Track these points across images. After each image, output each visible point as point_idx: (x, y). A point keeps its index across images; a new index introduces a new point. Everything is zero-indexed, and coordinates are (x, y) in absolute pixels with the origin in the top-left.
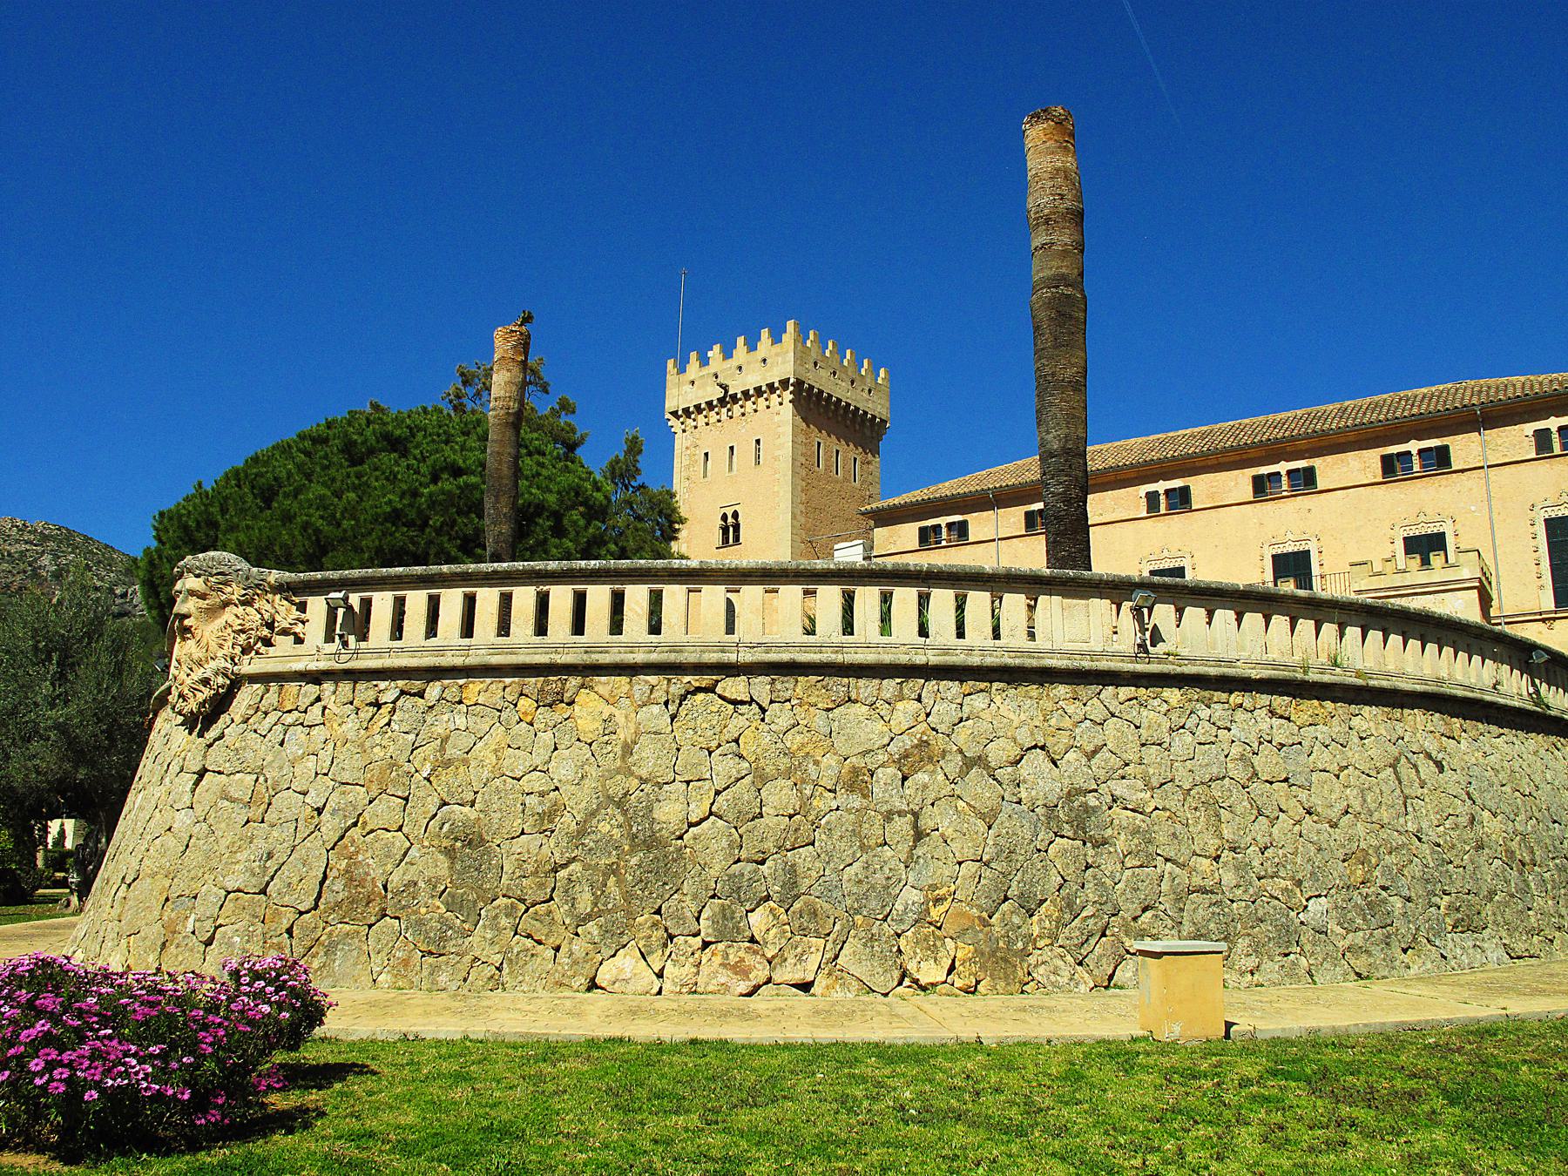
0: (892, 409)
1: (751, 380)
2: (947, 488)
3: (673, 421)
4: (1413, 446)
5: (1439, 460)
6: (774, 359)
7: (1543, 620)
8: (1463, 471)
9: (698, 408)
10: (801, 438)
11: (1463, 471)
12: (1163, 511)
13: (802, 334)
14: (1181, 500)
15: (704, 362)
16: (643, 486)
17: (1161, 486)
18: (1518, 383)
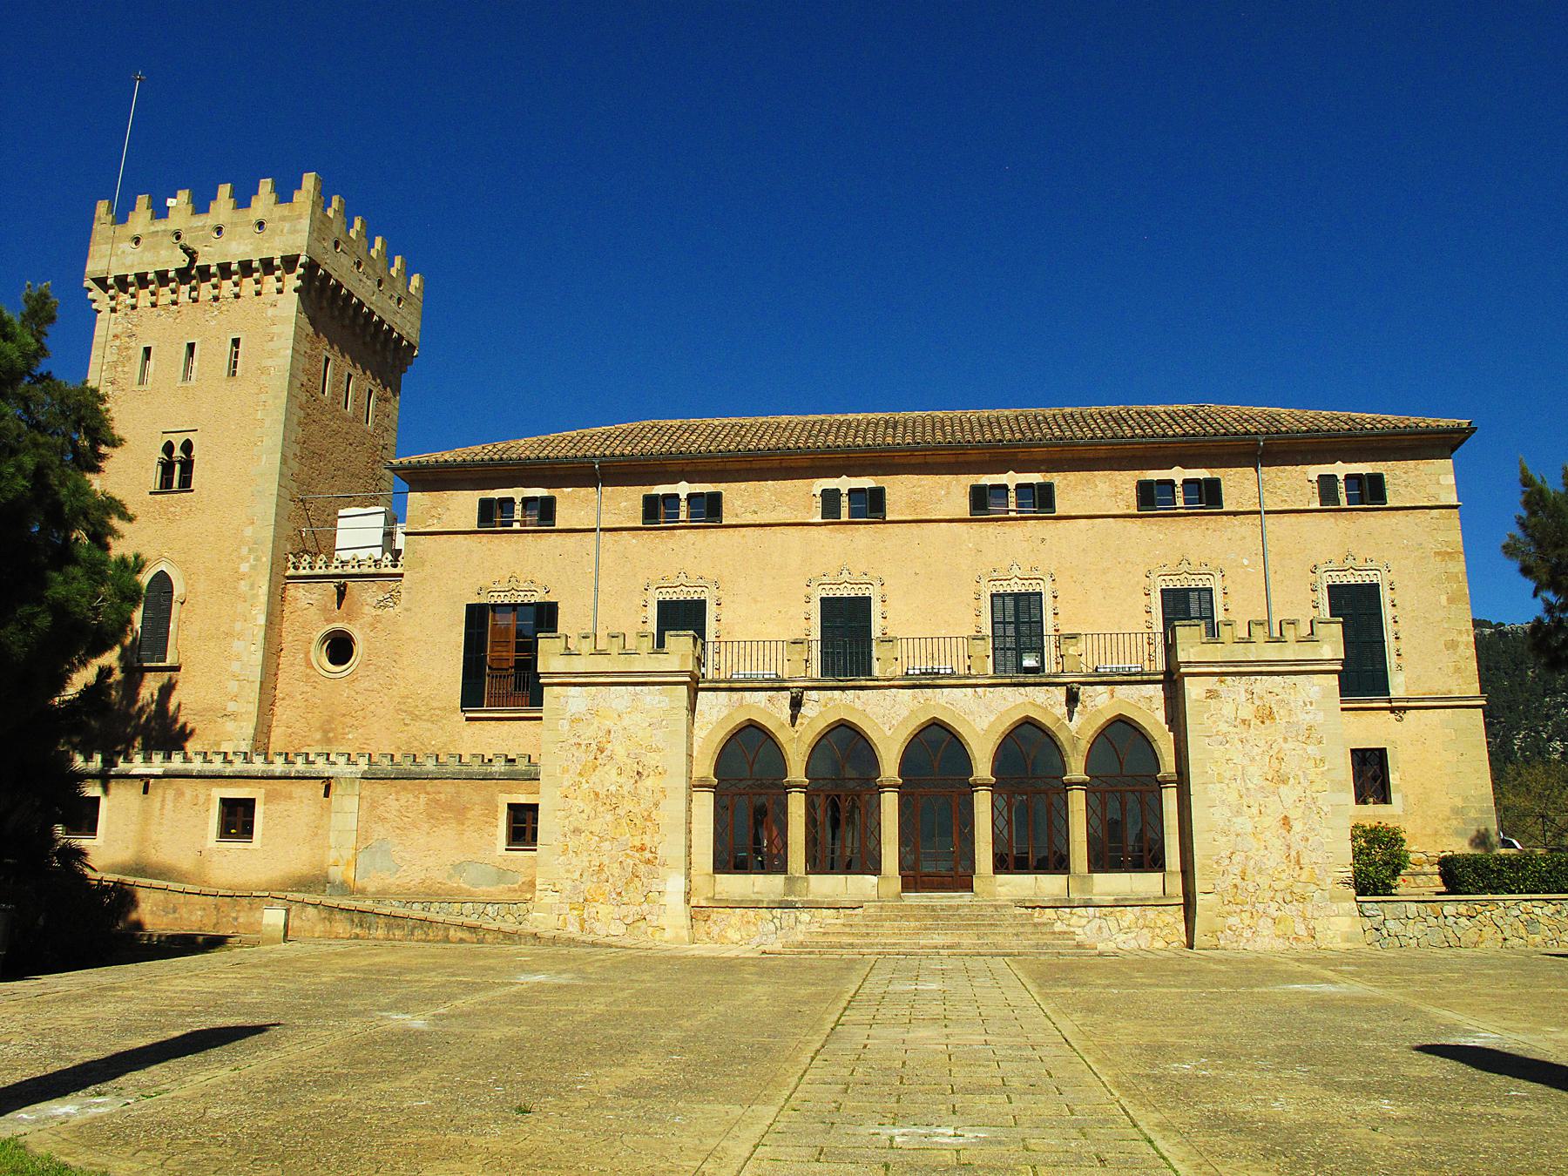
1: (238, 248)
2: (524, 447)
3: (96, 293)
4: (1178, 474)
5: (1208, 496)
6: (283, 223)
7: (1392, 710)
8: (1235, 514)
9: (142, 281)
10: (305, 346)
11: (1235, 514)
12: (845, 517)
14: (871, 506)
15: (160, 212)
16: (47, 377)
17: (844, 484)
18: (1290, 417)
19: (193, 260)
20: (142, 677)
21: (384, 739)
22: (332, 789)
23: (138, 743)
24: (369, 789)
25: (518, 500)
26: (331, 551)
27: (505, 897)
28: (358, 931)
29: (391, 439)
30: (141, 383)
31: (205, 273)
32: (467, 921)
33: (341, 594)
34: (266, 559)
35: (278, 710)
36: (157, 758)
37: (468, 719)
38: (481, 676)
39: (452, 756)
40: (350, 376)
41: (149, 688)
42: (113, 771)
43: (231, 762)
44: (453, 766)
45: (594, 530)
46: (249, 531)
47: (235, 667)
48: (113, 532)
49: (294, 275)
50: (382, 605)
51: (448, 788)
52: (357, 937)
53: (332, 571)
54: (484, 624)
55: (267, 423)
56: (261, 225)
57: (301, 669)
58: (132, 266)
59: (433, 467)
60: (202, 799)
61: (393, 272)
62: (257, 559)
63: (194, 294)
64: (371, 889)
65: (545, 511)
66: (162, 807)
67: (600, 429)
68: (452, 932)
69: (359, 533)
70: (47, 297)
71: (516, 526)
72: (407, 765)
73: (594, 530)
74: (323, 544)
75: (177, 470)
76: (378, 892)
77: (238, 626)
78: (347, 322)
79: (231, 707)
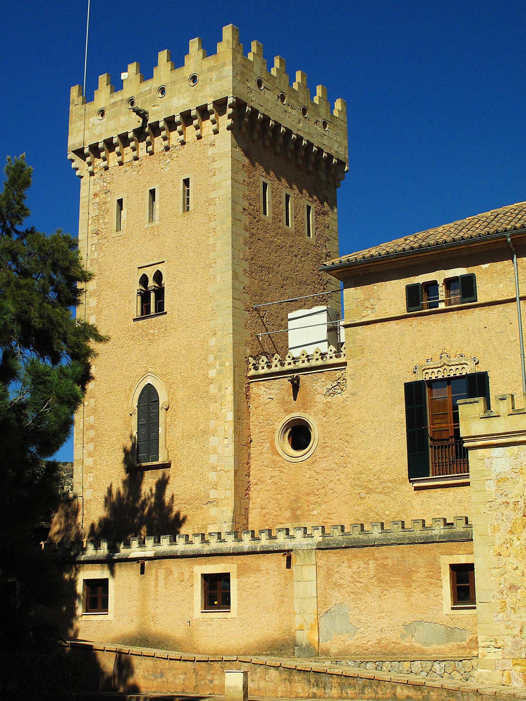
0: (351, 147)
1: (178, 102)
2: (442, 233)
3: (78, 163)
6: (211, 73)
9: (110, 145)
10: (243, 176)
13: (242, 45)
15: (117, 85)
16: (32, 231)
19: (145, 120)
20: (142, 475)
21: (341, 512)
22: (293, 561)
23: (144, 531)
24: (324, 558)
25: (440, 282)
26: (284, 350)
27: (454, 654)
28: (315, 690)
29: (333, 247)
30: (119, 229)
31: (156, 129)
32: (413, 678)
33: (296, 386)
34: (229, 364)
35: (253, 494)
36: (165, 541)
37: (416, 489)
38: (424, 448)
39: (395, 523)
40: (287, 197)
41: (149, 483)
42: (117, 556)
43: (207, 542)
44: (397, 532)
45: (514, 300)
46: (212, 342)
47: (213, 459)
48: (89, 352)
49: (226, 116)
50: (331, 392)
51: (392, 554)
52: (314, 696)
53: (287, 367)
54: (421, 399)
55: (218, 246)
56: (194, 79)
57: (268, 456)
58: (101, 134)
59: (361, 263)
60: (187, 575)
61: (316, 100)
62: (222, 364)
63: (150, 148)
64: (334, 650)
65: (466, 288)
66: (157, 583)
67: (513, 206)
68: (399, 690)
69: (306, 331)
70: (23, 167)
71: (442, 306)
72: (356, 534)
73: (514, 300)
74: (278, 346)
75: (152, 298)
76: (340, 653)
77: (212, 424)
78: (278, 149)
79: (213, 494)
